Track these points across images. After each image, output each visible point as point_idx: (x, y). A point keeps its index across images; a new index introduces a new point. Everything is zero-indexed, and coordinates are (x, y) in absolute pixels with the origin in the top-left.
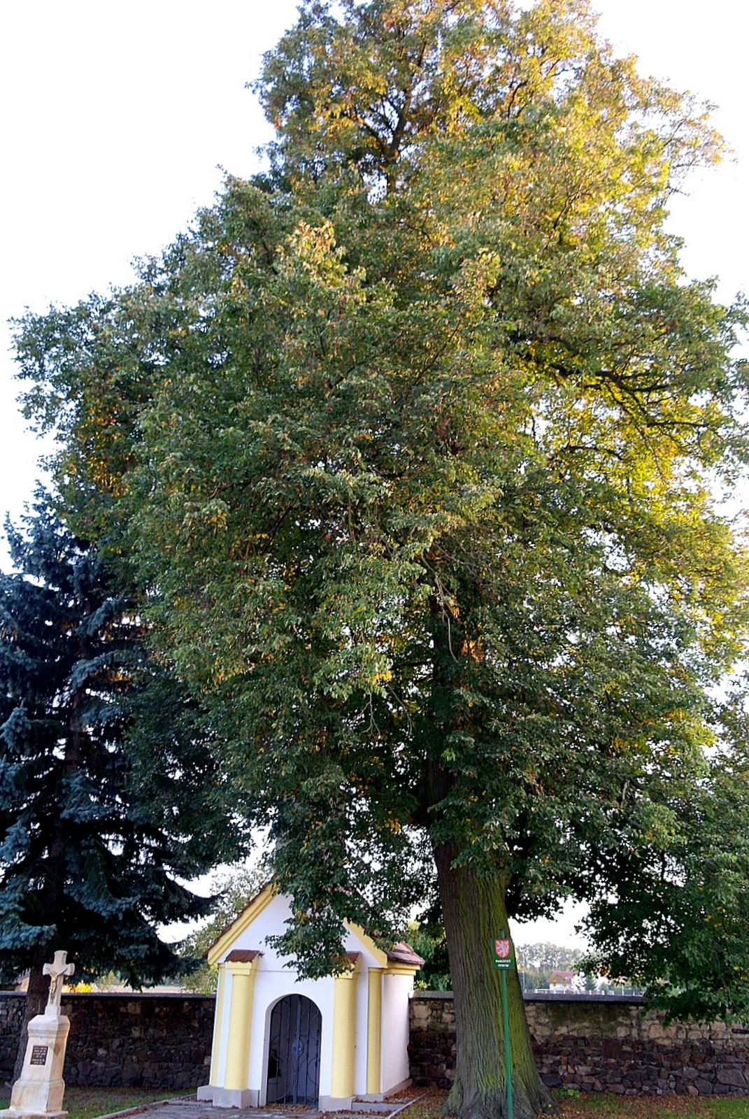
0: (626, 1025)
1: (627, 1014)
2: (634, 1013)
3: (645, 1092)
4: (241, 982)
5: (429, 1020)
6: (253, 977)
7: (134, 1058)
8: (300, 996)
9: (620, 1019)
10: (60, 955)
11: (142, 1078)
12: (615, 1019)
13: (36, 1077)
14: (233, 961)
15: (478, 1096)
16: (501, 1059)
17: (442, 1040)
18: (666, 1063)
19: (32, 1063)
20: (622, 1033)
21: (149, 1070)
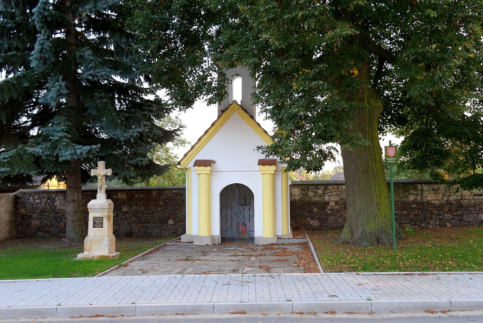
0: (414, 194)
1: (416, 189)
2: (419, 188)
3: (423, 227)
4: (204, 178)
5: (300, 196)
6: (210, 175)
7: (126, 222)
8: (237, 184)
9: (411, 192)
10: (101, 164)
11: (132, 232)
12: (408, 191)
13: (98, 234)
14: (199, 166)
15: (365, 233)
16: (378, 213)
17: (308, 206)
18: (436, 213)
19: (94, 227)
20: (411, 198)
21: (135, 228)
